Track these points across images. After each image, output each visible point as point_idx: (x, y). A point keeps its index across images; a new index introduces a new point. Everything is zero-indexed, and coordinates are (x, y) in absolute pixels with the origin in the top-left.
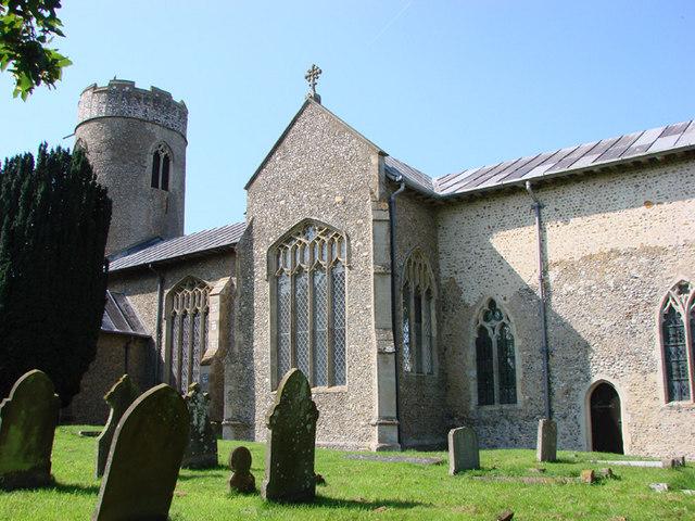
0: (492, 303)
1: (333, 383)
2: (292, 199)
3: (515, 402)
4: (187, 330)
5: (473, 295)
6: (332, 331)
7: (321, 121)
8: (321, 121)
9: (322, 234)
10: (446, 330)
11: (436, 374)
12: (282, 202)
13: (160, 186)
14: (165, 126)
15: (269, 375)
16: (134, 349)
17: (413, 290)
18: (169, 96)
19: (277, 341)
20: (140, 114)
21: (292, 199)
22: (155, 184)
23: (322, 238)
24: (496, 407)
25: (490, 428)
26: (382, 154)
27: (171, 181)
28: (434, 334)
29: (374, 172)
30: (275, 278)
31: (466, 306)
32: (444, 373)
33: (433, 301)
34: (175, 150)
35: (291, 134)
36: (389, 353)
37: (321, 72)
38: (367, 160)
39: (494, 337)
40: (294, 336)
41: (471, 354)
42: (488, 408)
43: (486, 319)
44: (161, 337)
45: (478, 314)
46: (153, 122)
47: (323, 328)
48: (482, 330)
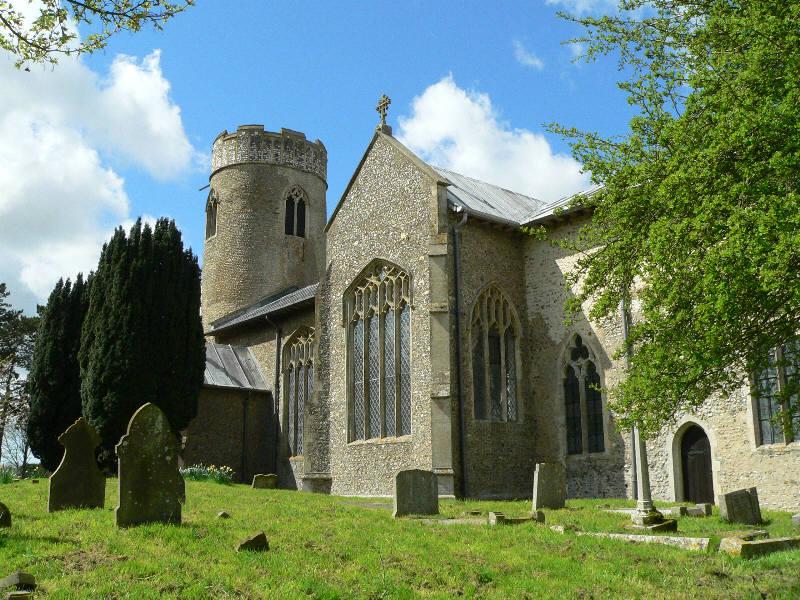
0: (578, 339)
1: (400, 433)
2: (364, 238)
3: (603, 450)
4: (302, 383)
5: (556, 334)
6: (399, 376)
7: (388, 154)
8: (388, 154)
9: (390, 275)
10: (535, 372)
11: (521, 421)
12: (356, 243)
13: (295, 231)
14: (299, 169)
15: (346, 426)
16: (252, 406)
17: (487, 330)
18: (302, 136)
19: (352, 390)
20: (271, 159)
21: (364, 238)
22: (289, 231)
23: (391, 278)
24: (583, 457)
25: (578, 479)
26: (443, 185)
27: (307, 226)
28: (519, 376)
29: (434, 204)
30: (351, 325)
31: (553, 344)
32: (531, 419)
33: (517, 342)
34: (311, 194)
35: (363, 171)
36: (445, 398)
37: (390, 102)
38: (429, 192)
39: (581, 375)
40: (367, 383)
41: (558, 396)
42: (577, 457)
43: (574, 357)
44: (278, 392)
45: (564, 353)
46: (285, 165)
47: (391, 375)
48: (569, 370)
